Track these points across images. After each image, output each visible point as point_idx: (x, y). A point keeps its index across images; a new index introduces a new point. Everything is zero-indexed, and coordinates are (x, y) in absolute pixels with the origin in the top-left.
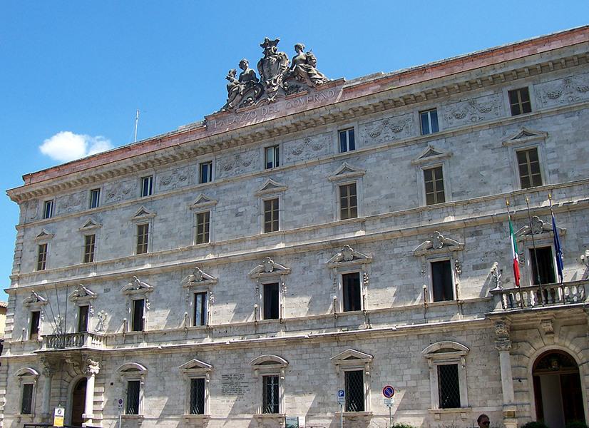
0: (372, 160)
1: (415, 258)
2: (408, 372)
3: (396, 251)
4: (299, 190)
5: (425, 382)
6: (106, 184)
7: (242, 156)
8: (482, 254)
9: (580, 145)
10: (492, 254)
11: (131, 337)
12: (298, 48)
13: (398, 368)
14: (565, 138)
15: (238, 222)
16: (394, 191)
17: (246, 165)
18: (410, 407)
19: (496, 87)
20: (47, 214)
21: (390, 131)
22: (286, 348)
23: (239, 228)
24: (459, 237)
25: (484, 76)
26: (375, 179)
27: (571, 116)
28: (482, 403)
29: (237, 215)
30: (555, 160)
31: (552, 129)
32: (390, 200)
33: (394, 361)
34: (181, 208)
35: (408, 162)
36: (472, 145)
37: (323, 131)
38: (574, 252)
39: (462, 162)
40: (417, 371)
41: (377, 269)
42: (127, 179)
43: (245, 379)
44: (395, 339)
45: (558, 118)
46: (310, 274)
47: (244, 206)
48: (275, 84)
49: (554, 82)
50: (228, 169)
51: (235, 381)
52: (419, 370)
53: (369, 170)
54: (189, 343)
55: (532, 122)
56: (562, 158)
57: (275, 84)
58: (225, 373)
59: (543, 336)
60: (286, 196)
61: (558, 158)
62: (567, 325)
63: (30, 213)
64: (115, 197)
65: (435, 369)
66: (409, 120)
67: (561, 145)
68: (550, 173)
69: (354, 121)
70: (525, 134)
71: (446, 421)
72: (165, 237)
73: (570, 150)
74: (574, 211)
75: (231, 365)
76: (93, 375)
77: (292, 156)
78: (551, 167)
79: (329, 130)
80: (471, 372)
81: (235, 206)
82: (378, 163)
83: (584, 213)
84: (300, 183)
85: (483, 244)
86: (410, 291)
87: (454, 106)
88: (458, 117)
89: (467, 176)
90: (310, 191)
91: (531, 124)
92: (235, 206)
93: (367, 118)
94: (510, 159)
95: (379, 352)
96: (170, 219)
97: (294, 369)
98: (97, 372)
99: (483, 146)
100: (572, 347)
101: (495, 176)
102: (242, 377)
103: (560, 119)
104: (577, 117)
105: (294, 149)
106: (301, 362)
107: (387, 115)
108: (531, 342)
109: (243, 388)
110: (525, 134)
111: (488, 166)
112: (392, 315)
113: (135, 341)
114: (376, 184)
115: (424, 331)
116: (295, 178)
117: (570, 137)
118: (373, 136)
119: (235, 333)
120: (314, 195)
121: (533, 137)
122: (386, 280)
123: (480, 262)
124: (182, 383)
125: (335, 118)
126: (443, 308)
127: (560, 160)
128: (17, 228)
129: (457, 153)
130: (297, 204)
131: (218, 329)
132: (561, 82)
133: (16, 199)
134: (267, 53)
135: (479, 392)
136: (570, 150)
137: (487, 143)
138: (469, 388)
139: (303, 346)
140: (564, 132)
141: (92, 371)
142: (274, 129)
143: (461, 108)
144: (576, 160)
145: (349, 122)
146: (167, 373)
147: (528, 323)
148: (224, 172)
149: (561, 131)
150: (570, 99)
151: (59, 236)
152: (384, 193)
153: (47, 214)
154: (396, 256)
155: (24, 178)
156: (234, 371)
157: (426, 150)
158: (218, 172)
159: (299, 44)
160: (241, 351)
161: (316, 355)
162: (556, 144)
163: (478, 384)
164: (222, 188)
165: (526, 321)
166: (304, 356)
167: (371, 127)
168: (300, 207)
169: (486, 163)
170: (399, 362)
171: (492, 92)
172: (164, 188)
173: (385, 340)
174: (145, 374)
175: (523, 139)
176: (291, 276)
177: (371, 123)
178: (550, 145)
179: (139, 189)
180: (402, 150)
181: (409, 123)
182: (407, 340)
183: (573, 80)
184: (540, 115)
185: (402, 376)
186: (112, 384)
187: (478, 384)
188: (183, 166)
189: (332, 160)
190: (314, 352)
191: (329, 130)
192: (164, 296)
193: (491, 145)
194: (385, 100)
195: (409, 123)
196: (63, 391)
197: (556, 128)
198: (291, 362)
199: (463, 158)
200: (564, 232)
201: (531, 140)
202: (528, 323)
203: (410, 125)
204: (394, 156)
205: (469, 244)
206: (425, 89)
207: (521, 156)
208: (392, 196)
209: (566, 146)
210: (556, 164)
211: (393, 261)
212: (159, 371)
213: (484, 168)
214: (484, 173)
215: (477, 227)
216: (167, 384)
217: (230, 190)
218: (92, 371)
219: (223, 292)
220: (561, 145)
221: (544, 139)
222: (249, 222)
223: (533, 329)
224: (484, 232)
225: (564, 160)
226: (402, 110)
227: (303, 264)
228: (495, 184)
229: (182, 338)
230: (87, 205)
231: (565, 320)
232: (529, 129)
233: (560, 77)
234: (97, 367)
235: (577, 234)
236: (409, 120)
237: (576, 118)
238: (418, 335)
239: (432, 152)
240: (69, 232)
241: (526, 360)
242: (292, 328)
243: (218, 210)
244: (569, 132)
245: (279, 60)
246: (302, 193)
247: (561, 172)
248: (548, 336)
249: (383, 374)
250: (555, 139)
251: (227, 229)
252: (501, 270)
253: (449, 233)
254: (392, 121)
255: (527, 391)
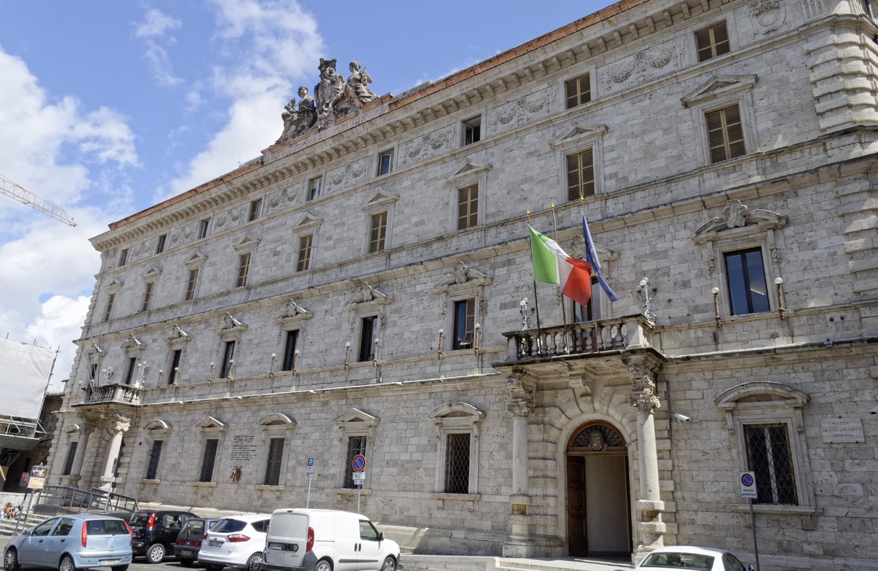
0: (407, 183)
1: (437, 296)
2: (414, 441)
3: (419, 288)
4: (333, 223)
5: (431, 454)
6: (172, 229)
7: (289, 190)
8: (512, 290)
9: (648, 138)
10: (525, 288)
11: (163, 390)
12: (352, 65)
13: (403, 435)
14: (630, 131)
15: (274, 262)
16: (425, 217)
17: (291, 199)
18: (411, 487)
19: (550, 78)
20: (123, 262)
21: (430, 147)
22: (297, 405)
23: (274, 268)
24: (487, 268)
25: (532, 63)
26: (407, 205)
27: (640, 101)
28: (494, 489)
29: (274, 255)
30: (614, 161)
31: (614, 121)
32: (419, 228)
33: (402, 426)
34: (228, 250)
35: (443, 181)
36: (516, 153)
37: (364, 155)
38: (629, 283)
39: (502, 176)
40: (424, 441)
41: (398, 311)
42: (189, 223)
43: (254, 442)
44: (405, 397)
45: (624, 105)
46: (331, 318)
47: (283, 244)
48: (327, 109)
49: (622, 61)
50: (275, 205)
51: (245, 443)
52: (427, 439)
53: (403, 195)
54: (211, 398)
55: (589, 115)
56: (623, 157)
57: (327, 109)
58: (237, 434)
59: (580, 400)
60: (321, 231)
61: (619, 157)
62: (613, 385)
63: (110, 262)
64: (177, 243)
65: (444, 438)
66: (450, 132)
67: (623, 140)
68: (605, 178)
69: (395, 140)
70: (579, 131)
71: (450, 511)
72: (211, 281)
73: (634, 145)
74: (633, 226)
75: (244, 424)
76: (121, 433)
77: (333, 186)
78: (608, 171)
79: (370, 153)
80: (485, 446)
81: (274, 246)
82: (412, 187)
83: (647, 228)
84: (336, 215)
85: (515, 276)
86: (427, 337)
87: (500, 109)
88: (503, 121)
89: (505, 192)
90: (343, 224)
91: (587, 118)
92: (274, 246)
93: (407, 136)
94: (558, 166)
95: (386, 414)
96: (217, 263)
97: (301, 431)
98: (126, 429)
99: (528, 153)
100: (618, 417)
101: (537, 189)
102: (252, 438)
103: (626, 106)
104: (649, 101)
105: (335, 178)
106: (309, 423)
107: (428, 129)
108: (562, 407)
109: (251, 453)
110: (579, 131)
111: (531, 177)
112: (405, 367)
113: (167, 396)
114: (407, 210)
115: (435, 388)
116: (331, 210)
117: (636, 130)
118: (412, 155)
119: (253, 387)
120: (346, 228)
121: (587, 134)
122: (404, 324)
123: (509, 299)
124: (199, 445)
125: (375, 138)
126: (460, 359)
127: (619, 161)
128: (96, 276)
129: (497, 165)
130: (329, 238)
131: (239, 383)
132: (631, 59)
133: (98, 247)
134: (323, 76)
135: (493, 473)
136: (634, 145)
137: (532, 149)
138: (480, 467)
139: (313, 404)
140: (629, 123)
141: (118, 428)
142: (315, 155)
143: (505, 110)
144: (642, 158)
145: (389, 142)
146: (187, 432)
147: (561, 380)
148: (271, 209)
149: (626, 121)
150: (641, 79)
151: (127, 284)
152: (414, 220)
153: (123, 262)
154: (417, 294)
155: (110, 226)
156: (245, 432)
157: (462, 165)
158: (265, 209)
159: (354, 62)
160: (255, 408)
161: (323, 415)
162: (617, 140)
163: (492, 462)
164: (266, 226)
165: (558, 378)
166: (313, 416)
167: (411, 145)
168: (331, 243)
169: (528, 174)
170: (405, 427)
171: (545, 85)
172: (219, 229)
173: (393, 398)
174: (168, 433)
175: (575, 138)
176: (312, 320)
177: (411, 141)
178: (610, 141)
179: (198, 232)
180: (439, 168)
181: (450, 136)
182: (418, 399)
183: (648, 53)
184: (599, 103)
185: (408, 445)
186: (140, 444)
187: (492, 462)
188: (238, 205)
189: (368, 187)
190: (322, 411)
191: (370, 153)
192: (199, 346)
193: (536, 151)
194: (423, 110)
195: (450, 136)
196: (101, 450)
197: (620, 119)
198: (299, 423)
199: (503, 171)
200: (615, 255)
201: (585, 138)
202: (561, 380)
203: (450, 138)
204: (430, 176)
205: (499, 276)
206: (465, 91)
207: (571, 162)
208: (422, 223)
209: (629, 141)
210: (615, 166)
211: (414, 301)
212: (181, 429)
213: (526, 180)
214: (525, 187)
215: (511, 254)
216: (186, 445)
217: (273, 228)
218: (118, 428)
219: (250, 340)
220: (623, 140)
221: (603, 134)
222: (284, 261)
223: (567, 388)
224: (518, 260)
225: (626, 160)
226: (444, 121)
227: (325, 307)
228: (537, 199)
229: (206, 392)
230: (154, 251)
231: (608, 377)
232: (582, 125)
233: (631, 53)
234: (128, 425)
235: (635, 257)
236: (450, 132)
237: (647, 102)
238: (430, 393)
239: (469, 167)
240: (135, 280)
241: (554, 433)
242: (306, 382)
243: (260, 249)
244: (634, 122)
245: (333, 82)
246: (336, 226)
247: (620, 176)
248: (584, 398)
249: (388, 441)
250: (617, 133)
251: (264, 270)
252: (655, 290)
253: (477, 264)
254: (434, 136)
255: (555, 478)
